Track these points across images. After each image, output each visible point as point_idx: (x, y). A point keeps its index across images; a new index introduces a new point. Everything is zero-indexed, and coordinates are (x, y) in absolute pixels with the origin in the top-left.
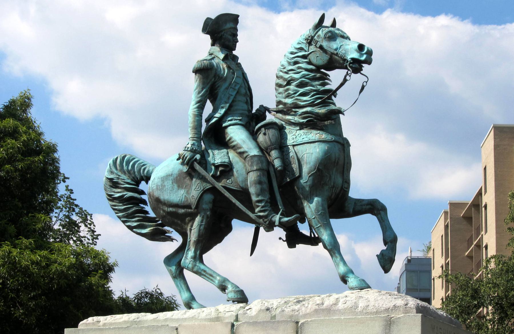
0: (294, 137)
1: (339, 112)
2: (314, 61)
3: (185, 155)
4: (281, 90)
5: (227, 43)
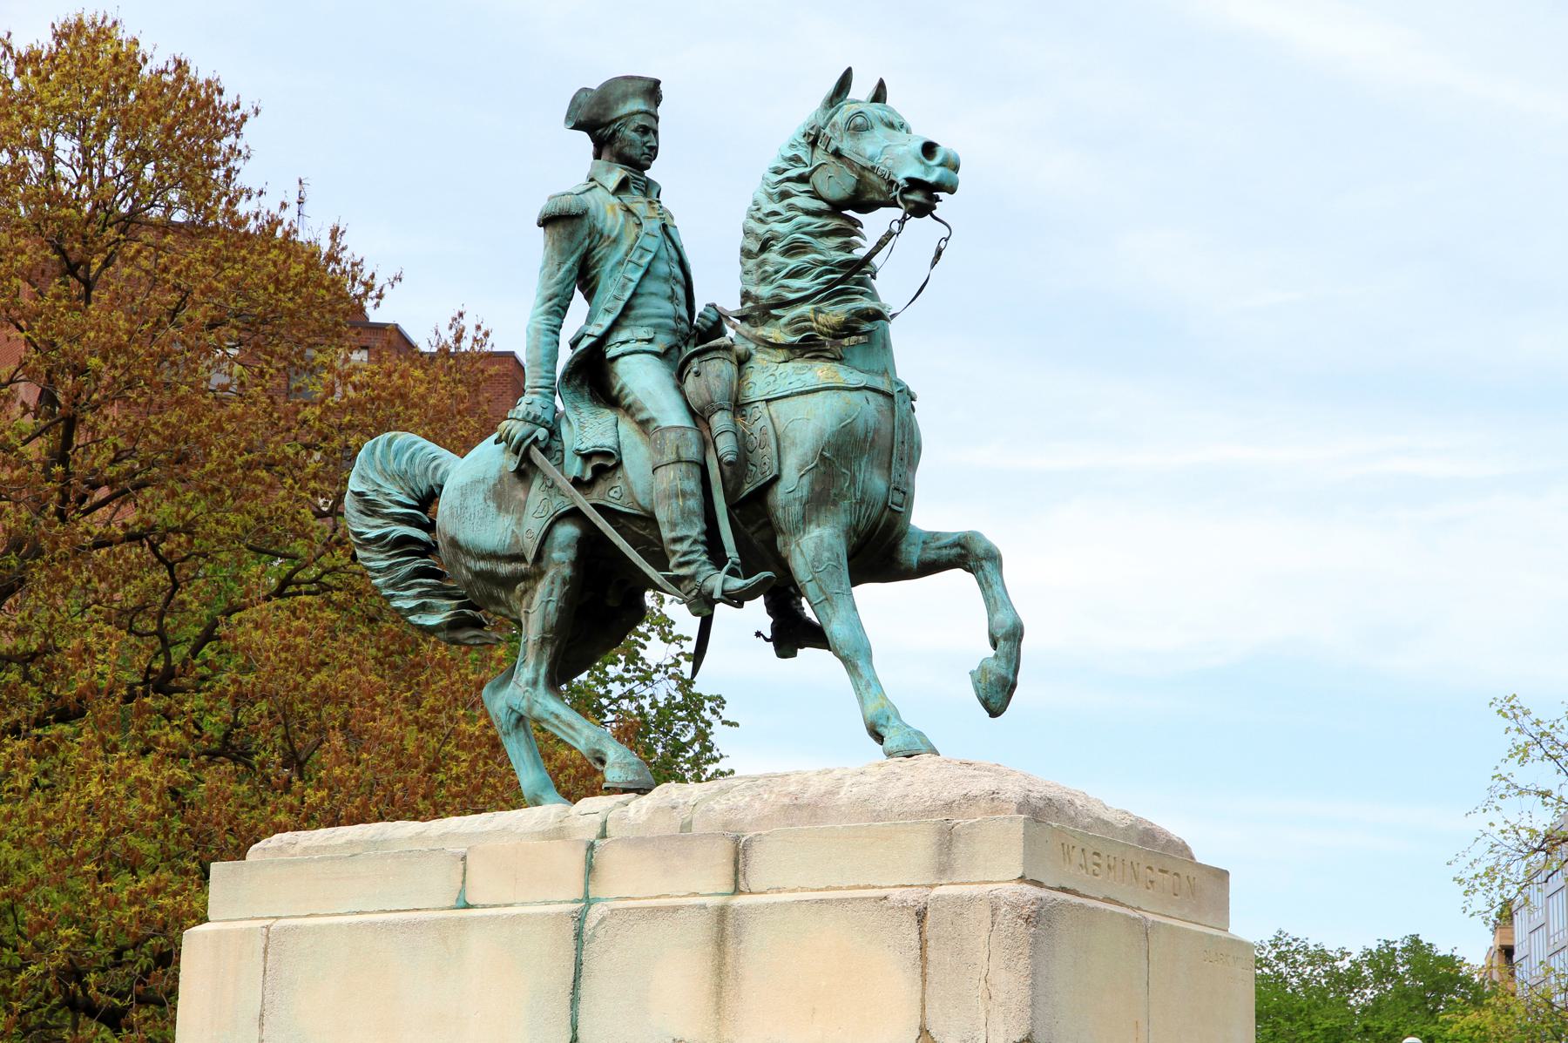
0: (772, 378)
1: (877, 316)
2: (825, 190)
4: (751, 263)
5: (627, 150)
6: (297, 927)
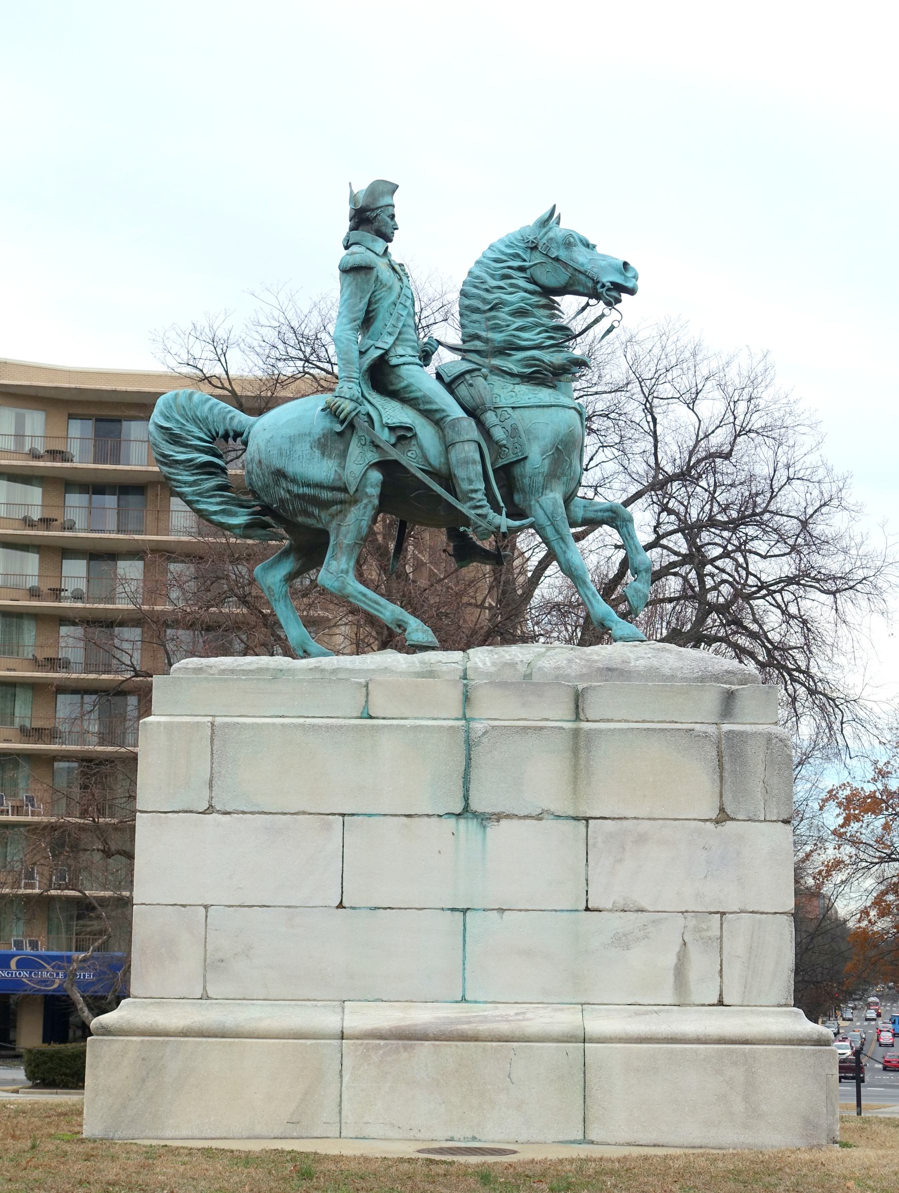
3: (339, 406)
6: (238, 723)
